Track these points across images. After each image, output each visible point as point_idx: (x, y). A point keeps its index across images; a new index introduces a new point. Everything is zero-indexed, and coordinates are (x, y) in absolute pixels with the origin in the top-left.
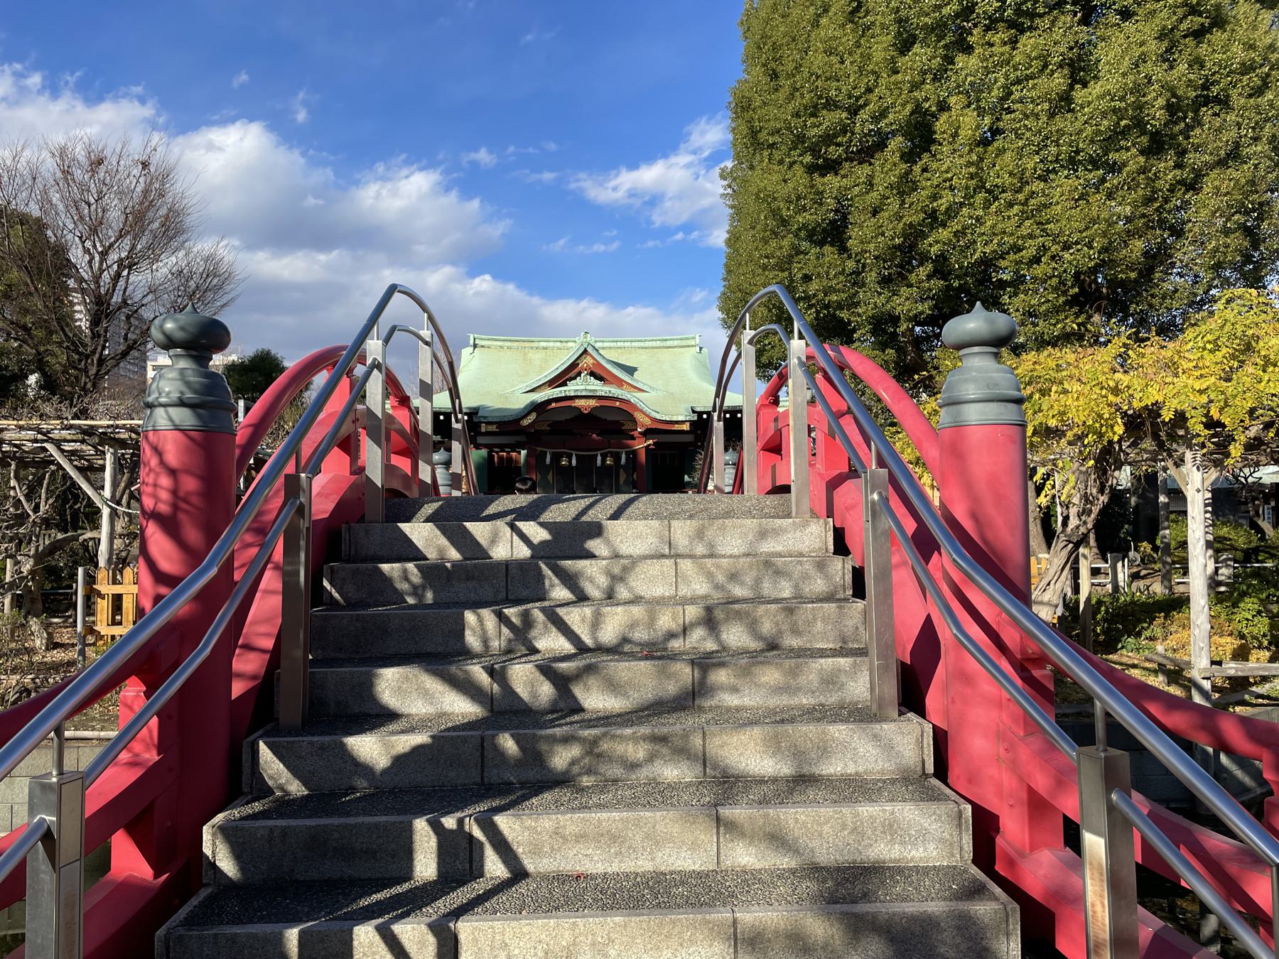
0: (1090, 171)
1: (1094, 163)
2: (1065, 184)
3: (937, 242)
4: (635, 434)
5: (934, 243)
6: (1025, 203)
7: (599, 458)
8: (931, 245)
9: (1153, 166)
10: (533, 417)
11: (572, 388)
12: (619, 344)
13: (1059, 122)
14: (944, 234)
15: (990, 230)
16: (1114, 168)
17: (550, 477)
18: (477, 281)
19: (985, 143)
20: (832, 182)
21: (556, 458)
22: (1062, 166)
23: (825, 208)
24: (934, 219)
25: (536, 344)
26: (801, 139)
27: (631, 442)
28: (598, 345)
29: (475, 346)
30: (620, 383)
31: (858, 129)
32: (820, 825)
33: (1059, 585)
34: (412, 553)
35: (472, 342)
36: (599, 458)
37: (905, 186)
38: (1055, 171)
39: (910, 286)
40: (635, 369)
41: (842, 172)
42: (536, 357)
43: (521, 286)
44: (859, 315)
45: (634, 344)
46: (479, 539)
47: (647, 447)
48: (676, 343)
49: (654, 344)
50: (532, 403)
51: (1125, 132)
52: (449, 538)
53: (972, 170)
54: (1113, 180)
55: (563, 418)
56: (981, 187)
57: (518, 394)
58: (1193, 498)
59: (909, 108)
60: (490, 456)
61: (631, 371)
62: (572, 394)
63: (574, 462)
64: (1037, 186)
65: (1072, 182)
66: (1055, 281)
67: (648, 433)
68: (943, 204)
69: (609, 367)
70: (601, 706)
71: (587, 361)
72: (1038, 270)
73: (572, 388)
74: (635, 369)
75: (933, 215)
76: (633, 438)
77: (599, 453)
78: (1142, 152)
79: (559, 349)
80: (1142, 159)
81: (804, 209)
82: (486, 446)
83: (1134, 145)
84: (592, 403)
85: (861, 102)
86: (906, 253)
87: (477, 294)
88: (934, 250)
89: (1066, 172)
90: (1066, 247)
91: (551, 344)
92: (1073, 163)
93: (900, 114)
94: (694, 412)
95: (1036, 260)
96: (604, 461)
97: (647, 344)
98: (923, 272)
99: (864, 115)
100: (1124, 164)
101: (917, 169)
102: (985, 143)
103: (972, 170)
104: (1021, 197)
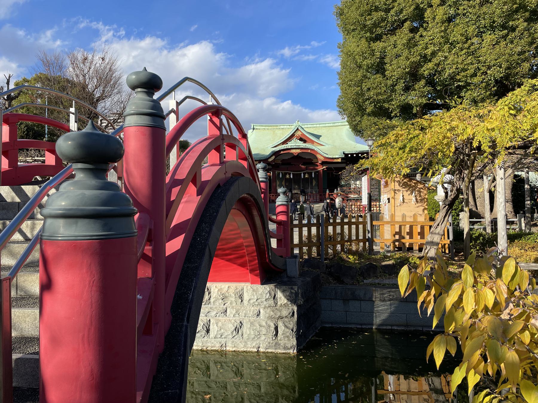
0: (501, 31)
1: (504, 27)
2: (489, 38)
3: (427, 69)
4: (318, 164)
5: (426, 69)
6: (469, 48)
7: (302, 175)
8: (424, 71)
9: (533, 27)
10: (273, 157)
11: (290, 145)
12: (314, 126)
13: (484, 9)
14: (430, 65)
15: (451, 63)
16: (513, 29)
18: (285, 103)
19: (450, 20)
20: (378, 46)
21: (284, 175)
22: (488, 30)
23: (375, 57)
24: (425, 59)
25: (279, 127)
26: (365, 26)
27: (316, 167)
28: (303, 127)
29: (254, 129)
30: (312, 142)
31: (390, 20)
32: (25, 317)
33: (443, 225)
35: (252, 127)
36: (302, 175)
37: (411, 44)
38: (484, 32)
39: (415, 90)
40: (320, 136)
41: (383, 40)
42: (278, 132)
43: (302, 106)
44: (393, 105)
45: (321, 125)
46: (27, 193)
48: (339, 124)
49: (330, 125)
50: (272, 152)
51: (517, 11)
52: (15, 193)
53: (442, 34)
54: (512, 35)
55: (287, 158)
56: (446, 42)
57: (269, 148)
58: (499, 182)
59: (413, 7)
61: (318, 137)
62: (290, 147)
63: (292, 176)
64: (475, 40)
65: (493, 37)
66: (484, 84)
67: (323, 163)
68: (429, 51)
69: (308, 135)
70: (7, 263)
71: (298, 133)
72: (476, 80)
73: (290, 145)
74: (320, 136)
75: (425, 56)
77: (302, 173)
78: (525, 21)
79: (288, 129)
80: (526, 24)
81: (366, 58)
83: (521, 17)
84: (299, 151)
85: (390, 7)
86: (414, 75)
87: (283, 109)
88: (426, 73)
89: (489, 32)
90: (489, 68)
91: (285, 127)
92: (492, 28)
93: (409, 10)
94: (344, 153)
95: (474, 75)
96: (304, 176)
98: (423, 82)
99: (392, 12)
100: (517, 27)
101: (417, 36)
102: (450, 20)
103: (442, 34)
104: (466, 46)
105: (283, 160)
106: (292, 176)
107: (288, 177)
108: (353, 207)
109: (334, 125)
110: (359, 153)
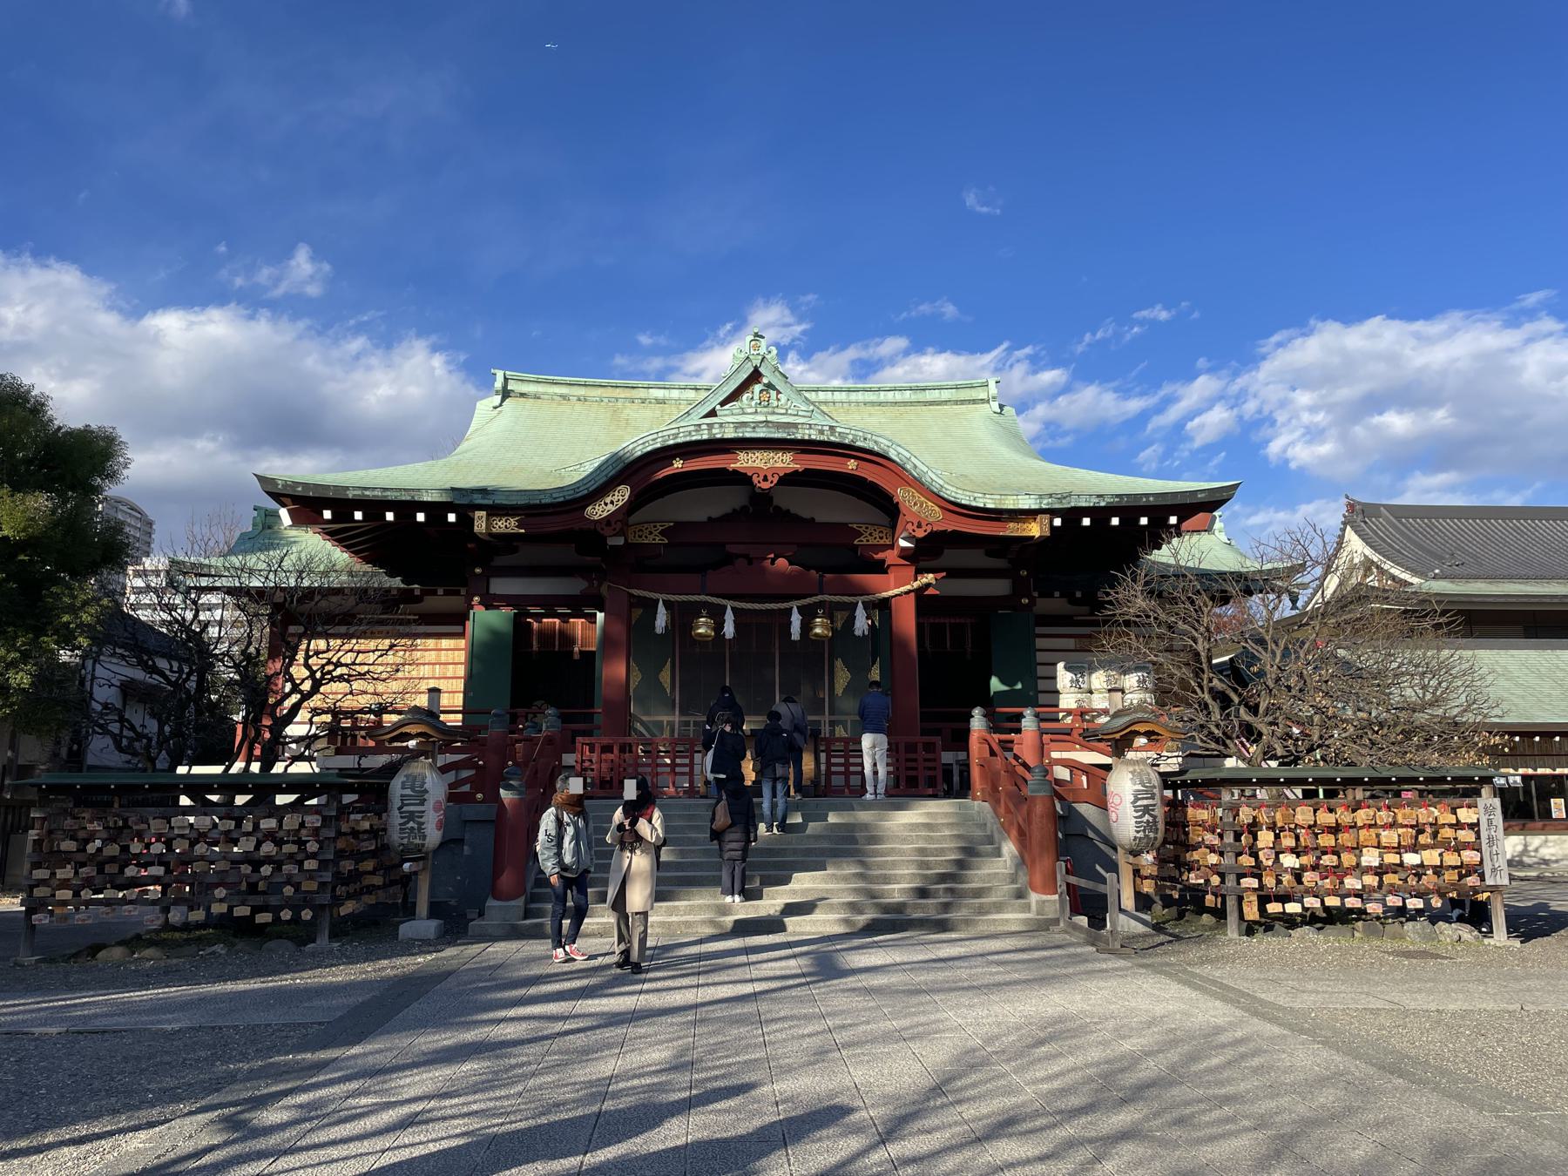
4: (890, 557)
7: (796, 619)
10: (621, 495)
17: (665, 677)
21: (683, 616)
25: (642, 393)
29: (506, 394)
34: (373, 873)
35: (498, 384)
36: (796, 619)
45: (853, 397)
47: (919, 592)
49: (898, 396)
60: (520, 625)
62: (730, 434)
63: (729, 630)
67: (928, 550)
76: (880, 568)
77: (794, 605)
82: (509, 600)
84: (784, 462)
91: (675, 394)
96: (806, 627)
97: (882, 396)
105: (680, 525)
106: (729, 630)
107: (703, 628)
108: (1265, 838)
109: (920, 396)
110: (1112, 510)
